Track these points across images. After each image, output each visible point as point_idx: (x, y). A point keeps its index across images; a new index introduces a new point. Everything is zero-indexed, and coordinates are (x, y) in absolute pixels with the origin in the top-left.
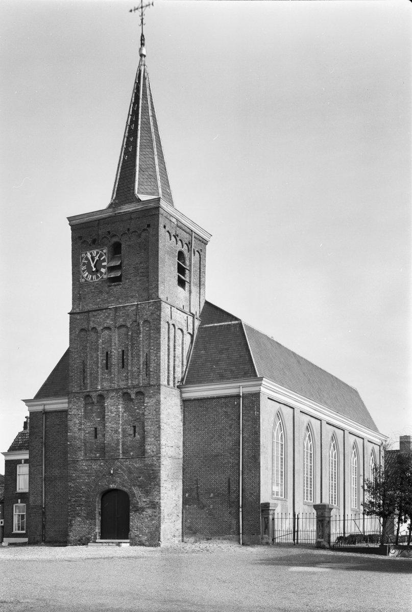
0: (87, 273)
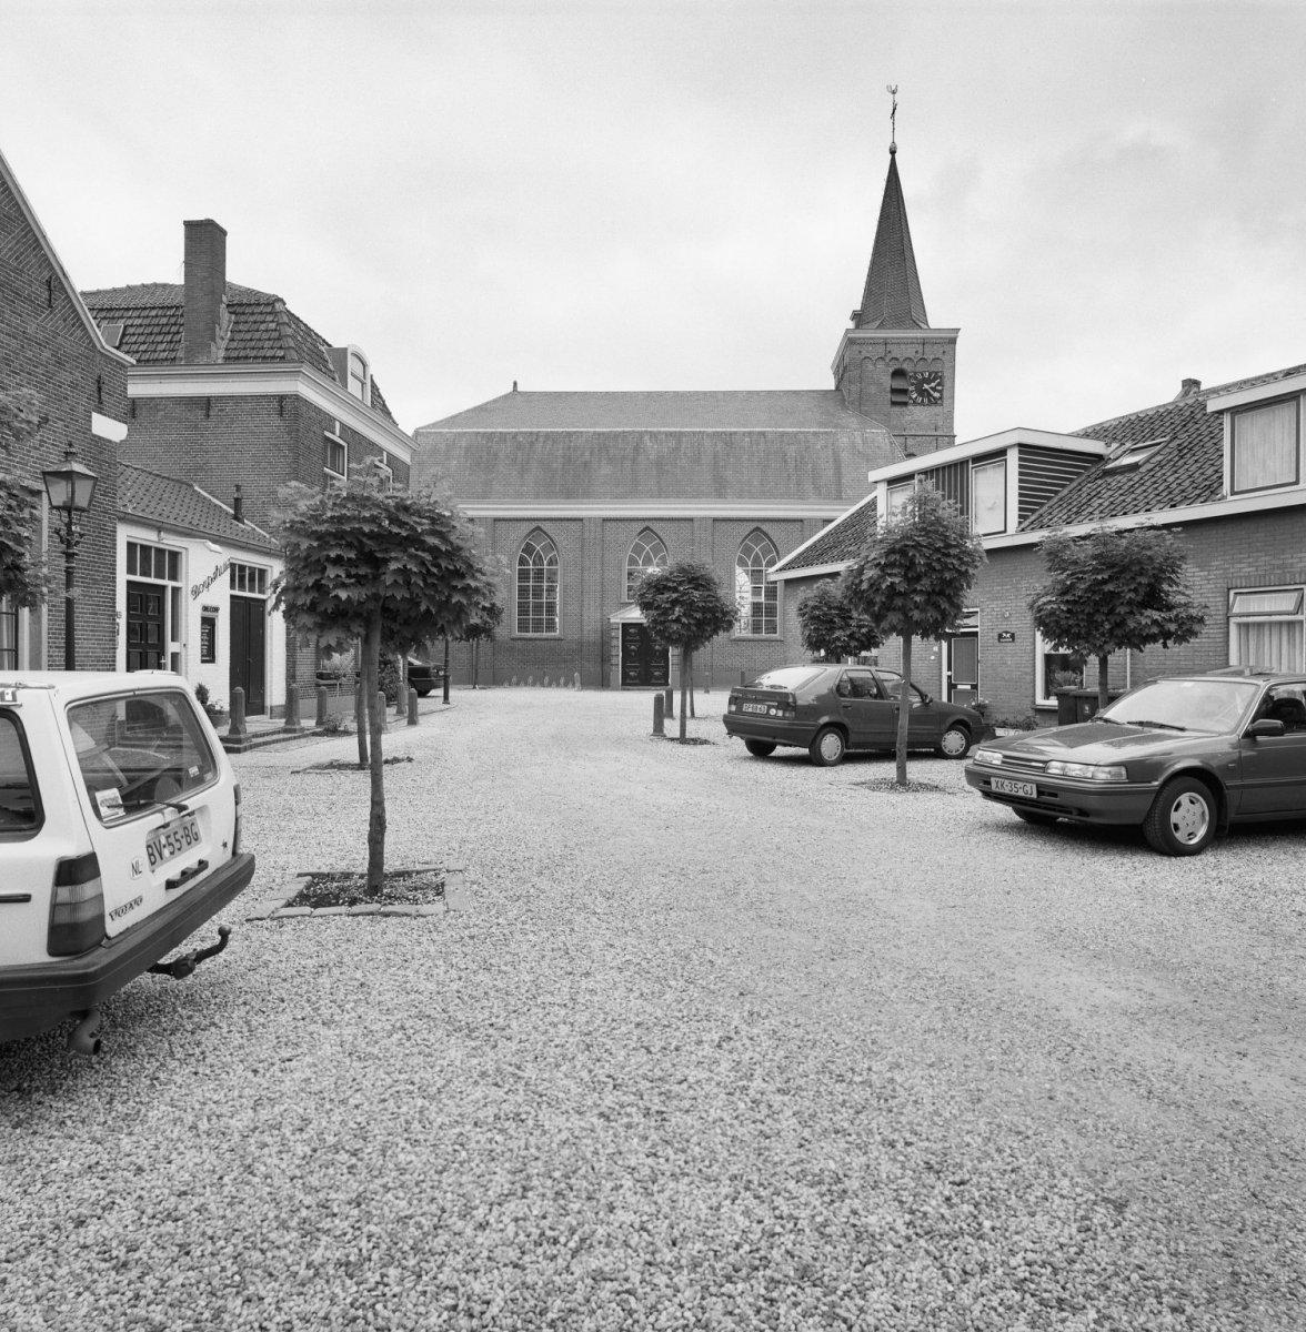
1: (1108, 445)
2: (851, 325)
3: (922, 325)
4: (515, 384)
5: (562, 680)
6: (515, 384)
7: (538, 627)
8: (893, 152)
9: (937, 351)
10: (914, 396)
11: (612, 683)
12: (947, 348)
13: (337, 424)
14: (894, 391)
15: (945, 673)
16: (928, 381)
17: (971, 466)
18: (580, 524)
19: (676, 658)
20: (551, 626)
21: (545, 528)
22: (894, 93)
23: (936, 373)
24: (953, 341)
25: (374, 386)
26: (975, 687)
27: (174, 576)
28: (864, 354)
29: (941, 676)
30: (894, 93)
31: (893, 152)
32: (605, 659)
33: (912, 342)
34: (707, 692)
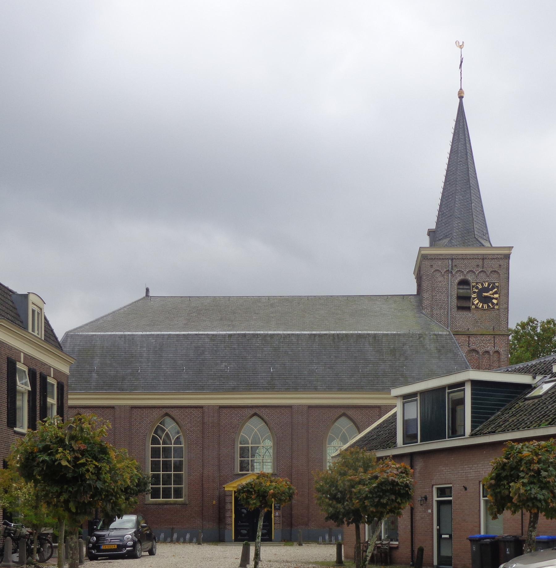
0: (477, 301)
1: (534, 378)
2: (426, 242)
3: (483, 242)
4: (147, 290)
5: (188, 536)
6: (147, 290)
7: (167, 494)
8: (461, 98)
9: (495, 265)
10: (475, 303)
11: (226, 538)
12: (501, 262)
13: (22, 355)
14: (459, 298)
15: (435, 527)
16: (487, 290)
17: (447, 391)
18: (200, 410)
19: (277, 518)
20: (178, 493)
21: (171, 413)
22: (461, 47)
23: (494, 283)
24: (507, 257)
25: (45, 318)
26: (451, 536)
27: (262, 540)
28: (435, 268)
29: (433, 529)
30: (461, 47)
31: (461, 98)
32: (221, 519)
33: (474, 257)
34: (300, 545)
